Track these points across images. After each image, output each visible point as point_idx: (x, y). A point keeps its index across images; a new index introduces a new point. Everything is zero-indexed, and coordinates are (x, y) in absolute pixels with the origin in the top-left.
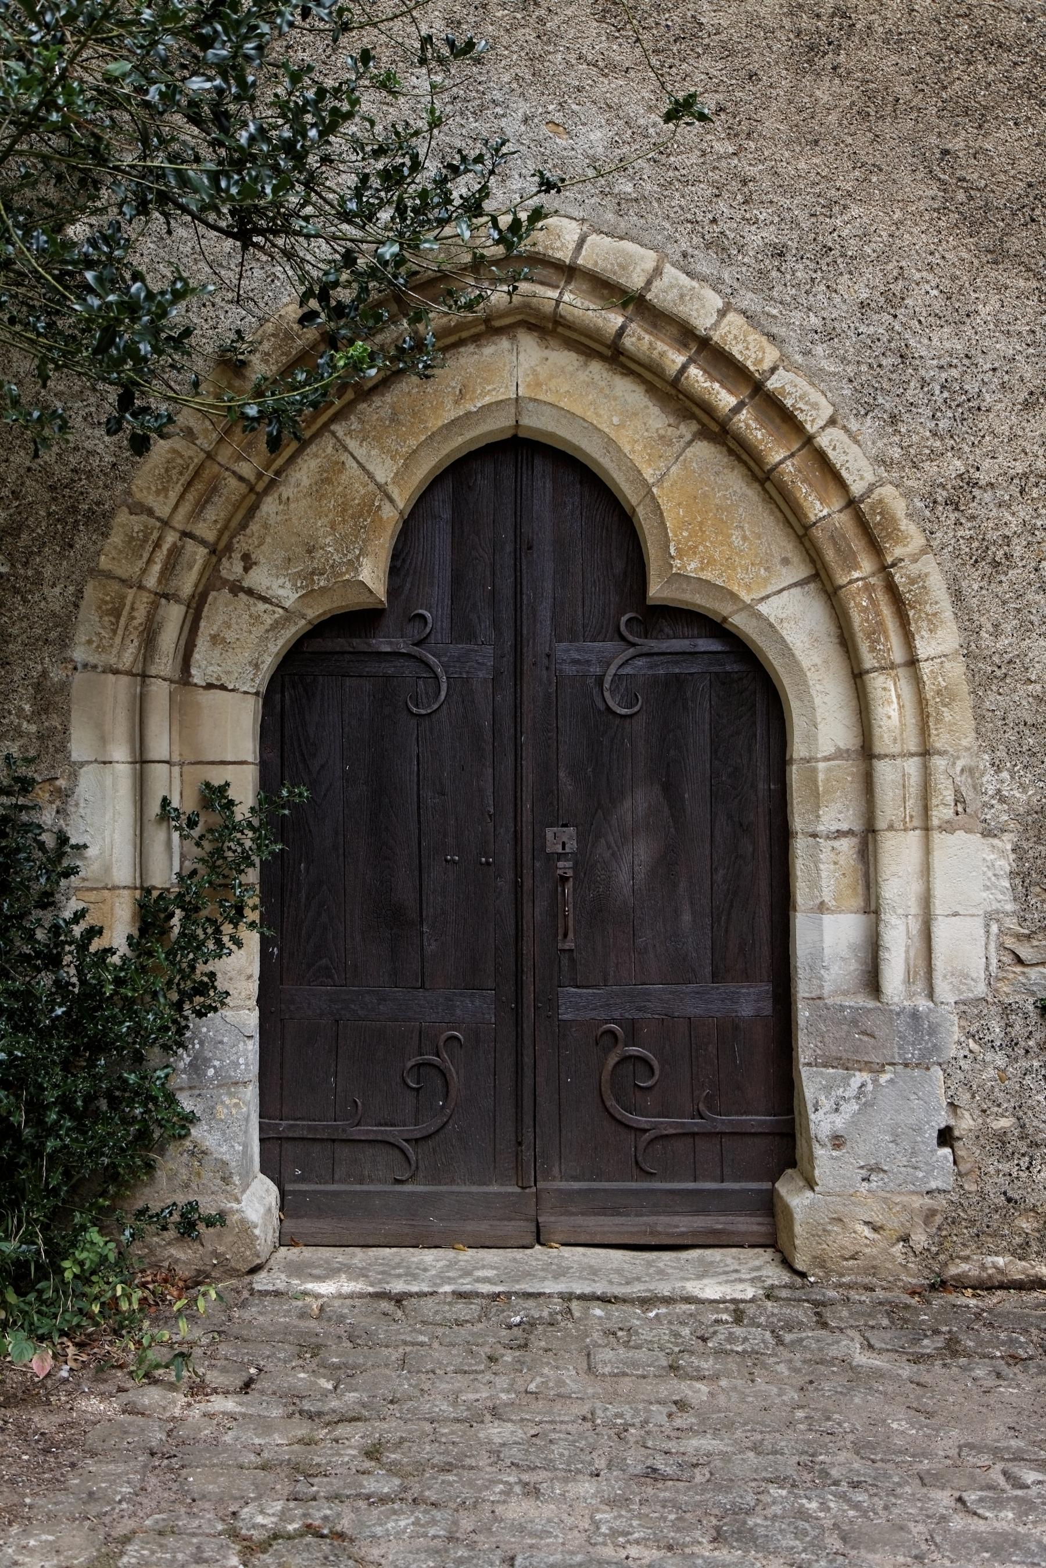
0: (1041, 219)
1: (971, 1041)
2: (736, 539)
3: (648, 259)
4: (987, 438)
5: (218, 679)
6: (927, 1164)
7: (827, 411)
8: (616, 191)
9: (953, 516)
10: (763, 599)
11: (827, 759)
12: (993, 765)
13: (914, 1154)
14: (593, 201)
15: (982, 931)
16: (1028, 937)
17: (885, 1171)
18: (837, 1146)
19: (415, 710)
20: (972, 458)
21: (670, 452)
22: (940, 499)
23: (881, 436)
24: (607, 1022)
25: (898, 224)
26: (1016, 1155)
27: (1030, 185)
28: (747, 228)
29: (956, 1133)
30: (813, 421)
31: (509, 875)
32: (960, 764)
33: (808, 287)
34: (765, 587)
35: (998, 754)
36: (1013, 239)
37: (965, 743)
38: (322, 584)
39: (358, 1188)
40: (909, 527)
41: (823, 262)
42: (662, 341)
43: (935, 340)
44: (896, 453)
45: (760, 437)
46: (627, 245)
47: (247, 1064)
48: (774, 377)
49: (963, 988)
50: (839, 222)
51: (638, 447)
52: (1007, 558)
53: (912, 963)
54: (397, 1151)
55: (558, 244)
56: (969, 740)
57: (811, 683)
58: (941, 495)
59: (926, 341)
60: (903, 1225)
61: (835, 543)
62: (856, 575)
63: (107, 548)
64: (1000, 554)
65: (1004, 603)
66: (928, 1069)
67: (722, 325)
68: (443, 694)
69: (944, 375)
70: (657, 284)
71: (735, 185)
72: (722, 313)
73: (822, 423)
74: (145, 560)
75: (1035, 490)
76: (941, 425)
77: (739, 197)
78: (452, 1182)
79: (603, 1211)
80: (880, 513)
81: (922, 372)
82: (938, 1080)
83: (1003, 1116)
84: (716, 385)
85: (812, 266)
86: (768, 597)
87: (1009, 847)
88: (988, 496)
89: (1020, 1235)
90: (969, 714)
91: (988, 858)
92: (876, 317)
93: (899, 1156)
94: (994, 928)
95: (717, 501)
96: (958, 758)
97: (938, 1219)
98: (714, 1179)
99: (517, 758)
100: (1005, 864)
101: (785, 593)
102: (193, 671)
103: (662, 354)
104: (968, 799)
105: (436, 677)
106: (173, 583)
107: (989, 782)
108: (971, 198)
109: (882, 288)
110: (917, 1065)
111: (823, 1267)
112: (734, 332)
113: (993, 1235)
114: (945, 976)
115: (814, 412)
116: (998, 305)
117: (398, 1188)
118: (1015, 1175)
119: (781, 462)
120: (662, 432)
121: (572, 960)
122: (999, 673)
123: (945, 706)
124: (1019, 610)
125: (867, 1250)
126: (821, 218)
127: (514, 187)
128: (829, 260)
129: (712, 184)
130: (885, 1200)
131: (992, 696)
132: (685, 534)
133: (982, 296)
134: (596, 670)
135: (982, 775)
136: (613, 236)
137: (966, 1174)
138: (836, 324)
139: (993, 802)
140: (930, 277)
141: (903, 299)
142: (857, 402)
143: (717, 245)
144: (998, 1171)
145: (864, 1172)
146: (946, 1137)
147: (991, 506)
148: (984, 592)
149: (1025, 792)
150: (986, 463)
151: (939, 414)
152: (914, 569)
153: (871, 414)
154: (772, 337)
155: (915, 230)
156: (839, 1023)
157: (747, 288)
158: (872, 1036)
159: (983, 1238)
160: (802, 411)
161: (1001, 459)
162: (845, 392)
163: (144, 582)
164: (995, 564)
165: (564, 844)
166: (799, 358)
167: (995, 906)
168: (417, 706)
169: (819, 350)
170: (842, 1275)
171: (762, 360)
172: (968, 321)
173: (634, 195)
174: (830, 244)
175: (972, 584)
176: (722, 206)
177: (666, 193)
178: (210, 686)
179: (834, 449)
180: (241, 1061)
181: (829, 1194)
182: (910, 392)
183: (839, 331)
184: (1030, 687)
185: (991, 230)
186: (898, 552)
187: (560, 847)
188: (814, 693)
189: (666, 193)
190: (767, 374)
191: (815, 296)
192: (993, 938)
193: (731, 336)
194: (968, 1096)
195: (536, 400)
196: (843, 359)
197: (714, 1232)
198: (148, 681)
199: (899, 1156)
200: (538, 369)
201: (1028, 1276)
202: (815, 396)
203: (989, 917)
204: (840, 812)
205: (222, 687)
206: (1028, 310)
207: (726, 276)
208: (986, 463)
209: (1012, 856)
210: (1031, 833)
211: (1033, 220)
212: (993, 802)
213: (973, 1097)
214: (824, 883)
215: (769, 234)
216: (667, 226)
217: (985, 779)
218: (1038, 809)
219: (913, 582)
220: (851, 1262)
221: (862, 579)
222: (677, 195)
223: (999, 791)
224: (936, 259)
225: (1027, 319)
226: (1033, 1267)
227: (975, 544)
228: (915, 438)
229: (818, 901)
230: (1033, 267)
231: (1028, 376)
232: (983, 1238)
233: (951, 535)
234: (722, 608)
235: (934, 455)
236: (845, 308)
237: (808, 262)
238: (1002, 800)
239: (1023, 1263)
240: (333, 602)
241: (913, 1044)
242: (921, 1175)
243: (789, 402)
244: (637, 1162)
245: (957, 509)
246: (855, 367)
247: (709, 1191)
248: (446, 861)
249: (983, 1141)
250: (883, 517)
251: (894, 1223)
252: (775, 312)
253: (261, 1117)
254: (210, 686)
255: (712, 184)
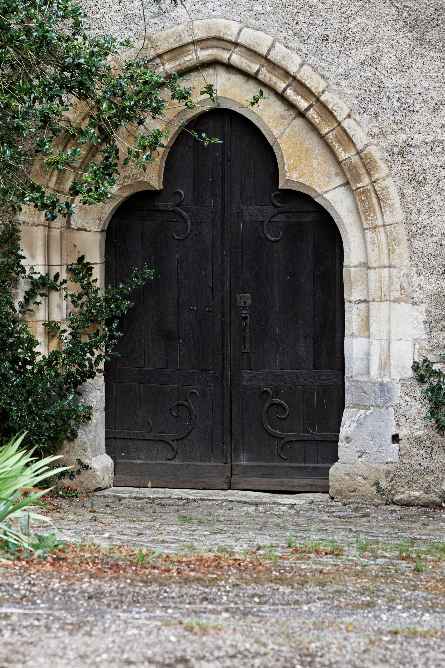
0: (441, 25)
1: (406, 396)
2: (315, 163)
3: (269, 40)
4: (417, 124)
5: (83, 226)
6: (386, 450)
7: (347, 111)
8: (254, 9)
9: (401, 160)
10: (327, 192)
11: (355, 267)
12: (417, 273)
13: (381, 446)
14: (244, 13)
15: (412, 347)
16: (432, 350)
17: (368, 453)
18: (348, 442)
19: (176, 237)
20: (410, 133)
21: (286, 122)
22: (395, 152)
23: (370, 123)
24: (265, 387)
25: (378, 26)
26: (425, 448)
27: (436, 10)
28: (312, 27)
29: (400, 437)
30: (340, 115)
31: (219, 317)
32: (403, 272)
33: (338, 55)
34: (328, 186)
35: (420, 268)
36: (428, 34)
37: (405, 263)
38: (129, 183)
39: (150, 462)
40: (382, 165)
41: (345, 44)
42: (277, 76)
43: (394, 79)
44: (376, 131)
45: (318, 122)
46: (259, 33)
47: (97, 402)
48: (324, 95)
49: (403, 372)
50: (352, 26)
51: (271, 120)
52: (424, 180)
53: (383, 361)
54: (168, 445)
55: (229, 33)
56: (407, 261)
57: (348, 231)
58: (396, 150)
59: (390, 80)
60: (376, 477)
61: (350, 171)
62: (359, 185)
63: (33, 171)
64: (421, 177)
65: (423, 200)
66: (387, 408)
67: (301, 71)
68: (189, 230)
69: (398, 96)
70: (273, 52)
71: (306, 8)
72: (302, 65)
73: (344, 116)
74: (49, 176)
75: (437, 148)
76: (397, 118)
77: (308, 13)
78: (193, 460)
79: (262, 476)
80: (369, 158)
81: (388, 94)
82: (391, 413)
83: (419, 430)
84: (299, 98)
85: (340, 45)
86: (329, 191)
87: (424, 310)
88: (416, 151)
89: (426, 483)
90: (407, 250)
91: (415, 315)
92: (368, 69)
93: (374, 447)
94: (417, 346)
95: (307, 146)
96: (402, 269)
97: (391, 475)
98: (302, 462)
99: (223, 261)
100: (423, 317)
101: (337, 189)
102: (72, 222)
103: (275, 83)
104: (406, 288)
105: (186, 222)
106: (62, 186)
107: (416, 281)
108: (410, 15)
109: (371, 56)
110: (383, 406)
111: (341, 495)
112: (306, 74)
113: (415, 483)
114: (395, 367)
115: (341, 111)
116: (422, 64)
117: (168, 462)
118: (424, 456)
119: (327, 134)
120: (282, 113)
121: (249, 358)
122: (420, 232)
123: (397, 246)
124: (429, 203)
125: (360, 488)
126: (344, 24)
127: (210, 7)
128: (347, 42)
129: (296, 7)
130: (368, 466)
131: (417, 242)
132: (292, 161)
133: (415, 60)
134: (260, 219)
135: (412, 277)
136: (254, 29)
137: (404, 455)
138: (350, 72)
139: (417, 290)
140: (392, 51)
141: (380, 61)
142: (360, 107)
143: (298, 35)
144: (417, 454)
145: (359, 454)
146: (395, 438)
147: (418, 155)
148: (414, 195)
149: (431, 285)
150: (416, 137)
151: (395, 113)
152: (383, 184)
153: (366, 113)
154: (323, 77)
155: (385, 30)
156: (357, 389)
157: (312, 54)
158: (366, 393)
159: (410, 483)
160: (336, 111)
161: (422, 134)
162: (354, 102)
163: (49, 185)
164: (419, 182)
165: (245, 302)
166: (334, 87)
167: (418, 336)
168: (177, 235)
169: (343, 83)
170: (349, 499)
171: (318, 87)
172: (408, 71)
173: (262, 12)
174: (347, 36)
175: (408, 191)
176: (301, 17)
177: (276, 11)
178: (79, 229)
179: (350, 128)
180: (94, 400)
181: (344, 463)
182: (383, 103)
183: (352, 75)
184: (433, 238)
185: (419, 30)
186: (377, 176)
187: (243, 303)
188: (349, 236)
189: (276, 11)
190: (321, 94)
191: (341, 58)
192: (416, 350)
193: (305, 76)
194: (404, 420)
195: (225, 98)
196: (354, 87)
197: (312, 486)
198: (51, 229)
199: (374, 447)
200: (226, 83)
201: (430, 501)
202: (341, 104)
203: (415, 341)
204: (361, 291)
205: (85, 230)
206: (435, 66)
207: (303, 49)
208: (416, 137)
209: (426, 314)
210: (433, 304)
211: (437, 25)
212: (417, 290)
213: (407, 421)
214: (353, 324)
215: (321, 31)
216: (277, 25)
217: (413, 279)
218: (437, 293)
219: (383, 189)
220: (354, 493)
221: (363, 187)
222: (281, 11)
223: (419, 285)
224: (393, 43)
225: (435, 70)
226: (432, 497)
227: (410, 173)
228: (385, 124)
229: (351, 332)
230: (437, 47)
231: (435, 96)
232: (410, 483)
233: (400, 168)
234: (312, 195)
235: (393, 132)
236: (354, 64)
237: (338, 43)
238: (421, 289)
239: (428, 495)
240: (134, 190)
241: (381, 397)
242: (384, 455)
243: (330, 107)
244: (278, 453)
245: (402, 157)
246: (359, 91)
247: (311, 467)
248: (191, 309)
249: (411, 441)
250: (370, 160)
251: (373, 477)
252: (324, 65)
253: (105, 428)
254: (79, 229)
255: (296, 7)
